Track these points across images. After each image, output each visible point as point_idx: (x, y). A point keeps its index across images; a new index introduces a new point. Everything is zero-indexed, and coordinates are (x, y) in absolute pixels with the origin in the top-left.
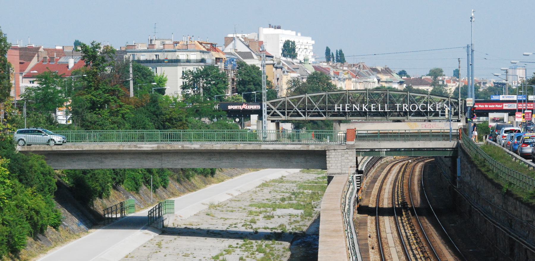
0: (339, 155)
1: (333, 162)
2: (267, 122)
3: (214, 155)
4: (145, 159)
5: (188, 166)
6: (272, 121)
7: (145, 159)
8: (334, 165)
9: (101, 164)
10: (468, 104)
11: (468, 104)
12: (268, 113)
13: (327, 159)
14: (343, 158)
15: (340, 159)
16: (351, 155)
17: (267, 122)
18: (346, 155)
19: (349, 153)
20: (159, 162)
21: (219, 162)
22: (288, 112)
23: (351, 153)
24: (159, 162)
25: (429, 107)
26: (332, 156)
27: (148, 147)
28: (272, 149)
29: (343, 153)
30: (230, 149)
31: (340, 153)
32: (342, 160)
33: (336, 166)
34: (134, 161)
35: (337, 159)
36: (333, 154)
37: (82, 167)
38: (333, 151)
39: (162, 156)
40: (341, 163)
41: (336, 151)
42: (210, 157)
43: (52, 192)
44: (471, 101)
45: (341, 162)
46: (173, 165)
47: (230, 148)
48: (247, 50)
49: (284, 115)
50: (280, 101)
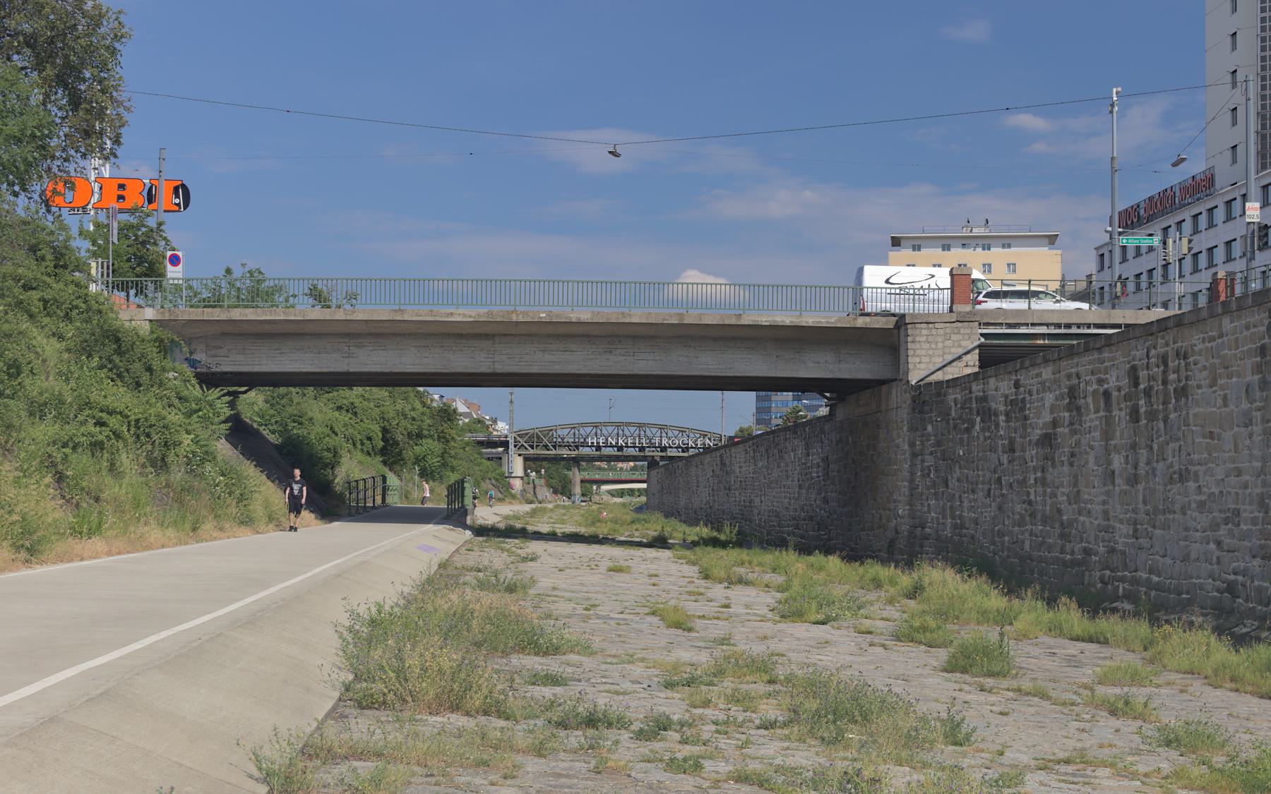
0: (937, 335)
1: (923, 352)
2: (514, 455)
3: (620, 341)
4: (454, 348)
5: (556, 367)
6: (520, 455)
7: (454, 348)
8: (925, 359)
9: (346, 361)
10: (1250, 216)
11: (1249, 216)
12: (515, 446)
13: (910, 346)
14: (948, 343)
15: (940, 345)
16: (967, 337)
17: (514, 455)
18: (954, 337)
19: (962, 331)
20: (486, 356)
21: (632, 358)
22: (537, 446)
23: (968, 331)
24: (486, 356)
25: (690, 443)
26: (923, 339)
27: (465, 315)
28: (768, 324)
29: (948, 331)
30: (665, 322)
31: (941, 332)
32: (944, 347)
33: (930, 362)
34: (427, 355)
35: (934, 346)
36: (925, 332)
37: (302, 366)
38: (923, 326)
39: (494, 344)
40: (943, 356)
41: (931, 326)
42: (610, 346)
43: (67, 17)
44: (1255, 209)
45: (944, 353)
46: (521, 363)
47: (664, 319)
48: (468, 410)
49: (533, 448)
50: (527, 434)
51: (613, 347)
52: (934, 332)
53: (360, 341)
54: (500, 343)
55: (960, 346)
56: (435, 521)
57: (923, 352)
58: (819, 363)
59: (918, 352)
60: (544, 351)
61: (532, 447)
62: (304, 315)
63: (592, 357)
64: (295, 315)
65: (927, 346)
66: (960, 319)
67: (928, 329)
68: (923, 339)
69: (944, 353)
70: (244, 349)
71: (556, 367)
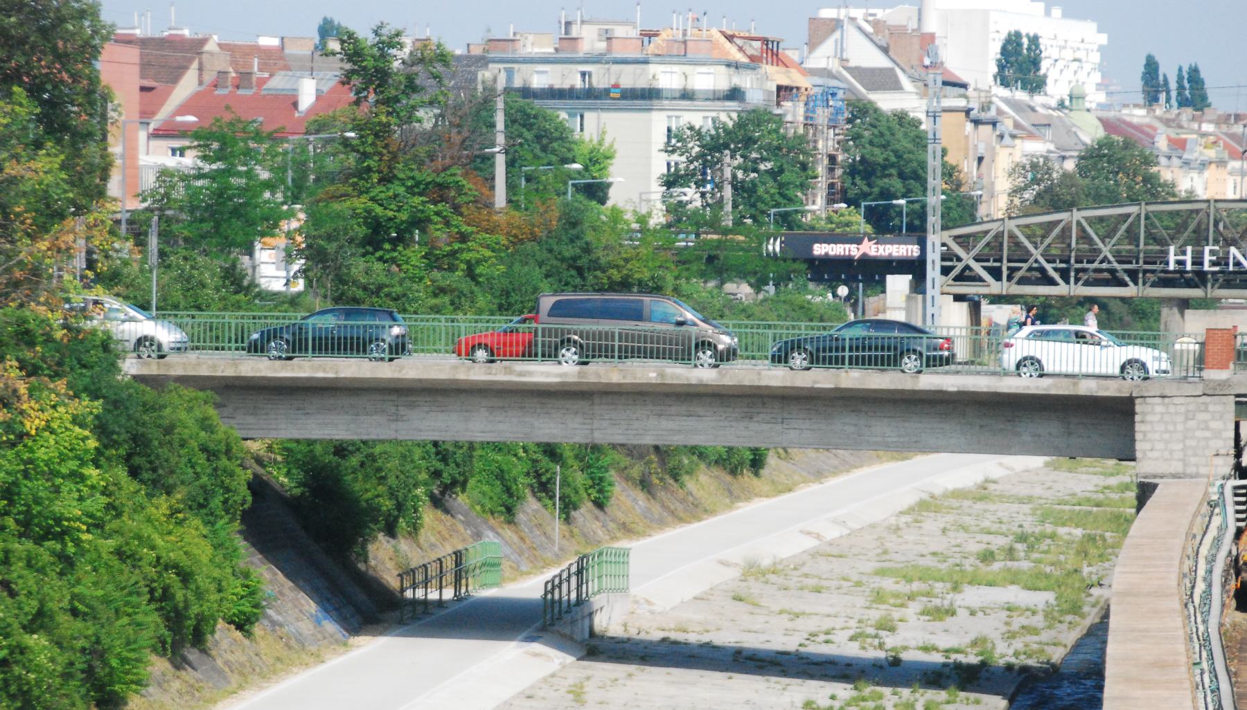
0: (1177, 413)
2: (939, 298)
5: (676, 438)
6: (958, 298)
9: (393, 426)
12: (945, 271)
14: (1191, 424)
17: (939, 298)
19: (1211, 408)
22: (1012, 271)
26: (1157, 418)
31: (1183, 409)
35: (1171, 428)
36: (1159, 409)
38: (1158, 400)
41: (1167, 400)
47: (815, 382)
48: (880, 61)
50: (986, 232)
51: (752, 410)
52: (1172, 409)
53: (413, 398)
54: (600, 404)
55: (1207, 428)
56: (524, 634)
57: (1157, 436)
58: (1039, 436)
59: (1149, 436)
60: (660, 415)
61: (996, 273)
62: (336, 373)
63: (726, 423)
64: (324, 371)
65: (1161, 427)
66: (1208, 392)
67: (1164, 404)
68: (1157, 418)
69: (1186, 438)
70: (255, 407)
71: (676, 438)
